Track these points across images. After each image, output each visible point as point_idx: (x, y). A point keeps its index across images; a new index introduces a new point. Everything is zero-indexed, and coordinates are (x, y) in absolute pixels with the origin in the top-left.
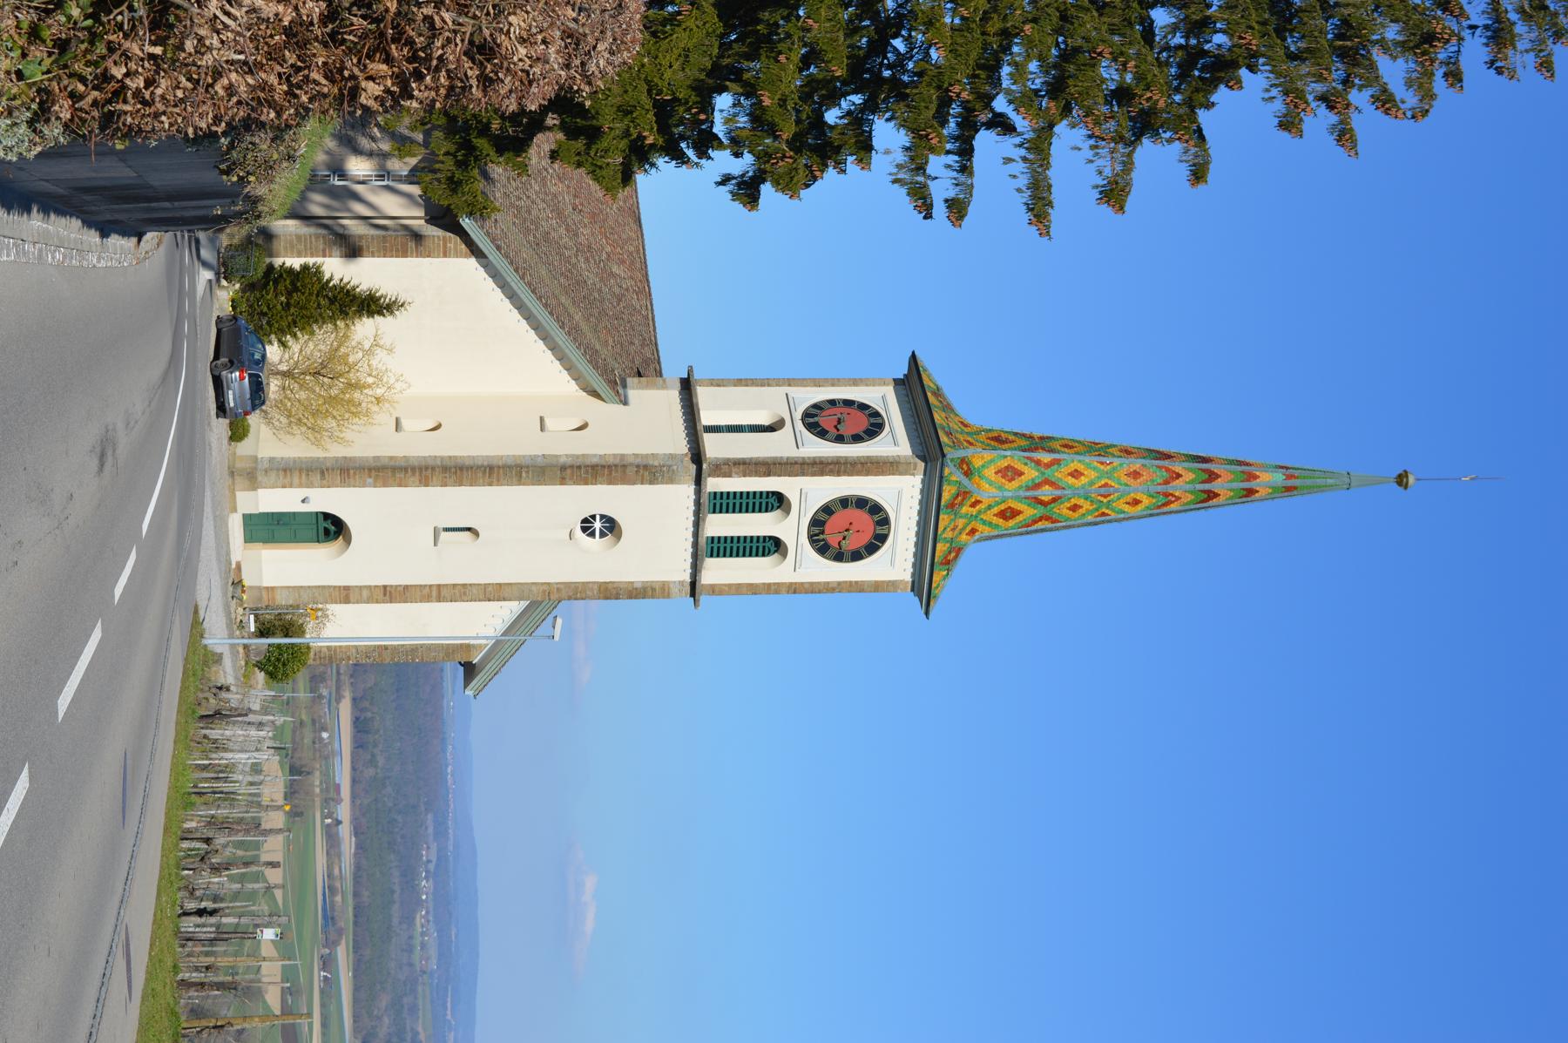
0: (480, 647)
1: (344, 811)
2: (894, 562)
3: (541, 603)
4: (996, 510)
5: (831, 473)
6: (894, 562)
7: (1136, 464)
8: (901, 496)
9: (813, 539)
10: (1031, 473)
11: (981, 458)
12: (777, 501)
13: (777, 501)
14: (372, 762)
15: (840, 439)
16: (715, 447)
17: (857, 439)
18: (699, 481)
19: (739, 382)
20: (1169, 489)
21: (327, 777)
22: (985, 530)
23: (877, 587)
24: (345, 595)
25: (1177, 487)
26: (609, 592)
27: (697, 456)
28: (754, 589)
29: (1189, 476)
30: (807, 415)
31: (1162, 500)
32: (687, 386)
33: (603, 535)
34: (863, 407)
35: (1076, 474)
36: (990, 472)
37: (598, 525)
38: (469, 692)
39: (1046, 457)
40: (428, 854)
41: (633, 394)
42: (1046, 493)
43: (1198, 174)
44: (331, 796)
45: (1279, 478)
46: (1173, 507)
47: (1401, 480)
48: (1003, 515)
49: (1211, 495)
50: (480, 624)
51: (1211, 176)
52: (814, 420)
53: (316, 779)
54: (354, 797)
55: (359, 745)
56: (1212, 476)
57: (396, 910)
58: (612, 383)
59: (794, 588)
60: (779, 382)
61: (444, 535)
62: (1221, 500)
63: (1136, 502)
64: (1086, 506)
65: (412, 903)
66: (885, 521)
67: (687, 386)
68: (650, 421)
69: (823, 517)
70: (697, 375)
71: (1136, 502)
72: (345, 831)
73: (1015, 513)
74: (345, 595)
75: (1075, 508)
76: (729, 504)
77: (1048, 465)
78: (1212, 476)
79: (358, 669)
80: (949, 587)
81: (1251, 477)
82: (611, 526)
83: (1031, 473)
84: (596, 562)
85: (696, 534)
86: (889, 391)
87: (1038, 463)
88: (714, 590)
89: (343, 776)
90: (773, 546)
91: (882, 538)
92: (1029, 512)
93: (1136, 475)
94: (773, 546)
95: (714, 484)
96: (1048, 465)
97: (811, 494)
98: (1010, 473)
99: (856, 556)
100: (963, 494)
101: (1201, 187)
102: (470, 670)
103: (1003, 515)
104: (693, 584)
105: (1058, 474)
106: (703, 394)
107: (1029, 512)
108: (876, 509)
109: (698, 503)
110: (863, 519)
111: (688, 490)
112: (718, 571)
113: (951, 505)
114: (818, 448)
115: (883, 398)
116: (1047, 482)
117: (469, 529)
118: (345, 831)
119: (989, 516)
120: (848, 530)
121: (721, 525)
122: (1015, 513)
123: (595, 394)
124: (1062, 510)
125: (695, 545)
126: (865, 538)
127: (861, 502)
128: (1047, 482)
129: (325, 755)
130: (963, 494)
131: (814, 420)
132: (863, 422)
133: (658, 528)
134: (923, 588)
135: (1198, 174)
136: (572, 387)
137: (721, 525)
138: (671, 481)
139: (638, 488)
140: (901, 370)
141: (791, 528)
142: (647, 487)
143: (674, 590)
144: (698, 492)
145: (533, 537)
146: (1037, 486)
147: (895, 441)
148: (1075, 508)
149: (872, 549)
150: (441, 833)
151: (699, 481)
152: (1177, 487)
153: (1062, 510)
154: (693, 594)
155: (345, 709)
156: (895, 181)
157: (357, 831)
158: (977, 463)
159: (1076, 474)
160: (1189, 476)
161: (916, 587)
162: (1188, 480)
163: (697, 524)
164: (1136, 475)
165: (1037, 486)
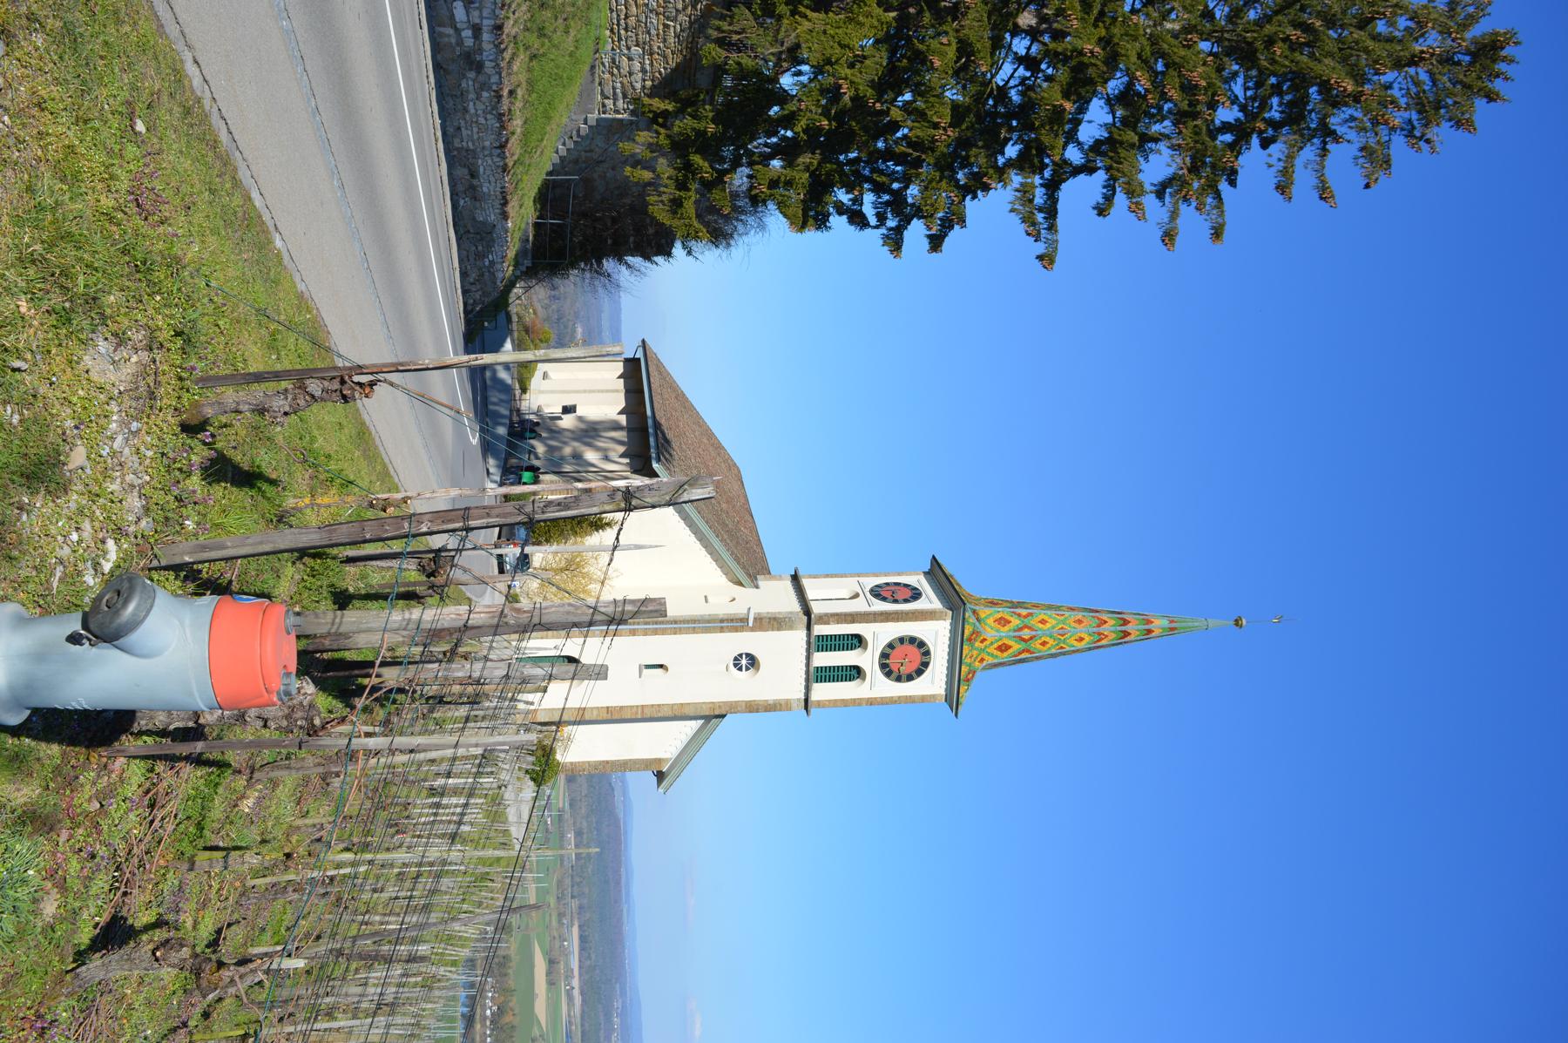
0: (666, 760)
1: (576, 982)
2: (933, 683)
3: (712, 717)
5: (893, 620)
6: (933, 683)
7: (1079, 615)
8: (937, 634)
9: (883, 666)
10: (1016, 622)
11: (984, 612)
12: (857, 641)
13: (857, 641)
14: (589, 958)
15: (896, 601)
16: (817, 609)
17: (906, 601)
18: (809, 627)
19: (827, 576)
20: (1101, 629)
21: (567, 964)
22: (991, 660)
23: (924, 699)
24: (582, 718)
25: (1105, 629)
26: (752, 707)
27: (807, 612)
28: (845, 703)
29: (1112, 622)
30: (872, 591)
31: (1097, 637)
32: (795, 579)
34: (906, 586)
35: (1043, 622)
36: (990, 621)
37: (744, 662)
38: (661, 790)
39: (1024, 612)
40: (617, 1004)
41: (761, 583)
42: (1026, 634)
43: (1217, 233)
44: (569, 975)
45: (1165, 623)
46: (1103, 642)
47: (1237, 622)
48: (999, 648)
49: (1126, 634)
50: (664, 741)
51: (1225, 236)
52: (877, 593)
53: (562, 966)
54: (580, 975)
55: (582, 949)
56: (1126, 622)
57: (602, 1034)
58: (749, 576)
59: (871, 702)
60: (852, 576)
61: (645, 671)
62: (1132, 638)
63: (1081, 639)
64: (1051, 642)
65: (610, 1031)
66: (927, 653)
67: (795, 579)
68: (775, 596)
69: (888, 651)
70: (801, 573)
71: (1081, 639)
72: (576, 992)
73: (1008, 647)
74: (582, 718)
75: (1044, 644)
76: (830, 643)
78: (1126, 622)
79: (590, 777)
80: (966, 695)
81: (1149, 622)
82: (753, 662)
83: (1016, 622)
84: (744, 687)
85: (808, 665)
86: (922, 579)
88: (819, 704)
89: (575, 965)
90: (856, 673)
91: (926, 665)
92: (1016, 646)
93: (1080, 622)
94: (856, 673)
95: (819, 630)
97: (880, 635)
98: (1003, 622)
99: (910, 678)
100: (976, 633)
101: (1218, 245)
102: (660, 776)
103: (999, 648)
104: (806, 700)
105: (1032, 622)
106: (806, 582)
107: (1016, 646)
108: (922, 644)
109: (809, 643)
110: (913, 650)
111: (802, 634)
112: (822, 691)
113: (970, 640)
114: (880, 606)
115: (918, 580)
116: (1026, 627)
117: (661, 666)
118: (576, 992)
119: (992, 650)
120: (904, 660)
121: (823, 659)
122: (1008, 647)
123: (741, 584)
124: (1036, 645)
125: (807, 672)
126: (916, 665)
127: (912, 640)
128: (1026, 627)
129: (566, 953)
130: (976, 633)
131: (877, 593)
132: (908, 594)
133: (784, 661)
134: (953, 699)
135: (1217, 233)
136: (723, 580)
137: (823, 659)
138: (791, 628)
139: (770, 633)
140: (927, 567)
141: (867, 659)
142: (776, 633)
143: (794, 705)
144: (809, 635)
145: (699, 670)
146: (1020, 629)
147: (930, 600)
148: (1044, 644)
149: (920, 672)
150: (623, 993)
151: (809, 627)
152: (1105, 629)
153: (1036, 645)
154: (806, 708)
155: (575, 930)
156: (1012, 211)
157: (582, 993)
158: (982, 616)
159: (1043, 622)
160: (1112, 622)
161: (948, 698)
162: (1111, 628)
163: (808, 658)
164: (1080, 622)
165: (1020, 629)
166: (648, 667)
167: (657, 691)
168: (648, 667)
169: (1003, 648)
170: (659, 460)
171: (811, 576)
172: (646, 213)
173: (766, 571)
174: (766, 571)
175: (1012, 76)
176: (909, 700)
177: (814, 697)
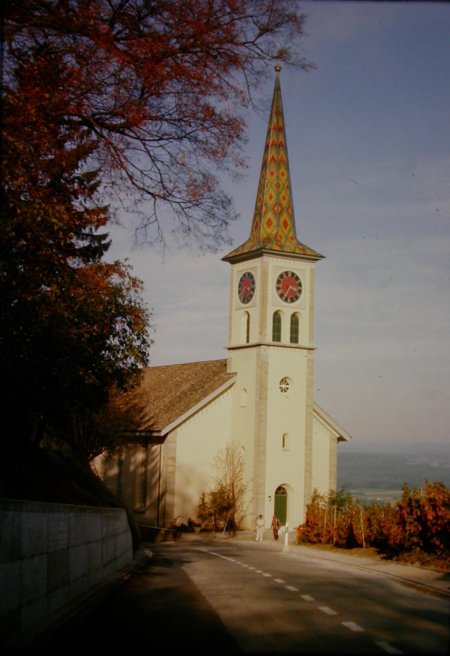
4: (284, 229)
6: (301, 268)
12: (277, 318)
13: (277, 318)
33: (288, 384)
35: (271, 197)
36: (269, 231)
37: (284, 386)
69: (289, 300)
77: (267, 208)
82: (284, 381)
87: (266, 212)
90: (295, 320)
94: (295, 320)
95: (269, 339)
96: (267, 208)
97: (274, 302)
106: (234, 344)
112: (304, 339)
113: (281, 246)
128: (273, 209)
133: (283, 361)
141: (287, 310)
145: (287, 412)
159: (271, 197)
166: (284, 446)
167: (296, 442)
168: (284, 446)
169: (285, 224)
170: (159, 431)
171: (230, 339)
172: (56, 270)
173: (224, 364)
174: (224, 364)
175: (154, 140)
176: (312, 286)
177: (306, 344)
